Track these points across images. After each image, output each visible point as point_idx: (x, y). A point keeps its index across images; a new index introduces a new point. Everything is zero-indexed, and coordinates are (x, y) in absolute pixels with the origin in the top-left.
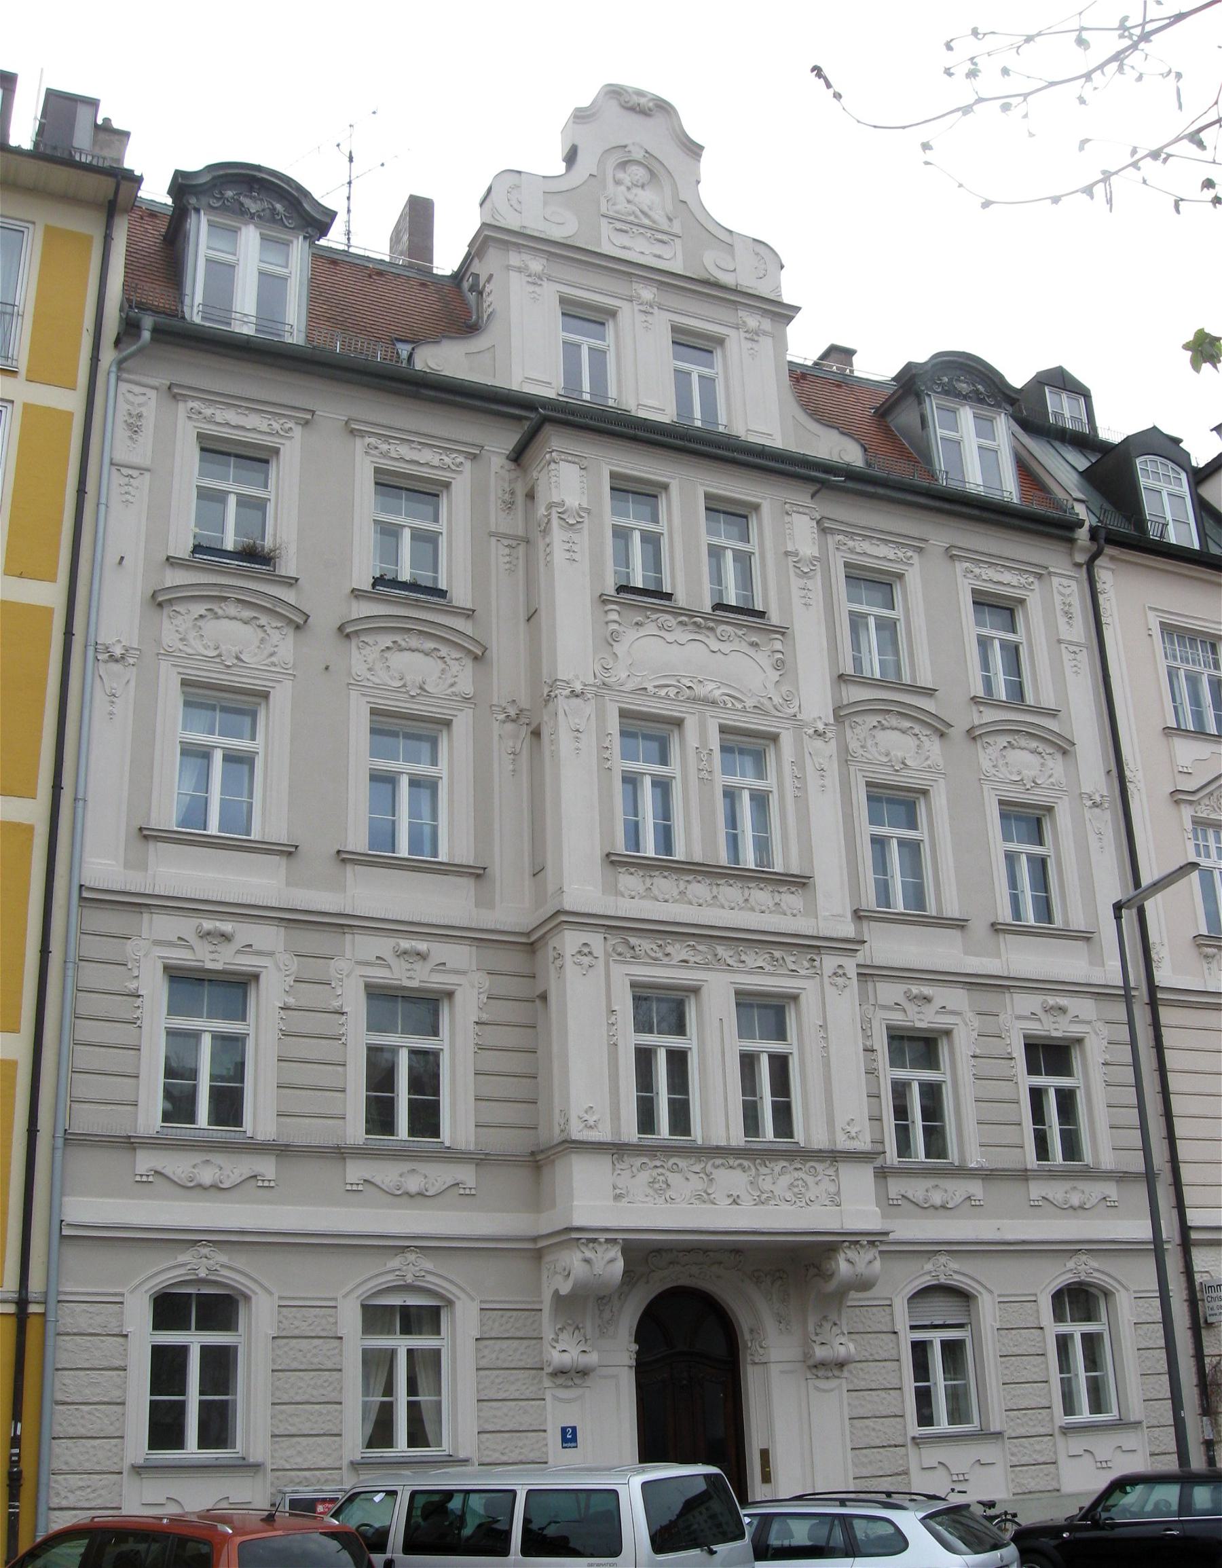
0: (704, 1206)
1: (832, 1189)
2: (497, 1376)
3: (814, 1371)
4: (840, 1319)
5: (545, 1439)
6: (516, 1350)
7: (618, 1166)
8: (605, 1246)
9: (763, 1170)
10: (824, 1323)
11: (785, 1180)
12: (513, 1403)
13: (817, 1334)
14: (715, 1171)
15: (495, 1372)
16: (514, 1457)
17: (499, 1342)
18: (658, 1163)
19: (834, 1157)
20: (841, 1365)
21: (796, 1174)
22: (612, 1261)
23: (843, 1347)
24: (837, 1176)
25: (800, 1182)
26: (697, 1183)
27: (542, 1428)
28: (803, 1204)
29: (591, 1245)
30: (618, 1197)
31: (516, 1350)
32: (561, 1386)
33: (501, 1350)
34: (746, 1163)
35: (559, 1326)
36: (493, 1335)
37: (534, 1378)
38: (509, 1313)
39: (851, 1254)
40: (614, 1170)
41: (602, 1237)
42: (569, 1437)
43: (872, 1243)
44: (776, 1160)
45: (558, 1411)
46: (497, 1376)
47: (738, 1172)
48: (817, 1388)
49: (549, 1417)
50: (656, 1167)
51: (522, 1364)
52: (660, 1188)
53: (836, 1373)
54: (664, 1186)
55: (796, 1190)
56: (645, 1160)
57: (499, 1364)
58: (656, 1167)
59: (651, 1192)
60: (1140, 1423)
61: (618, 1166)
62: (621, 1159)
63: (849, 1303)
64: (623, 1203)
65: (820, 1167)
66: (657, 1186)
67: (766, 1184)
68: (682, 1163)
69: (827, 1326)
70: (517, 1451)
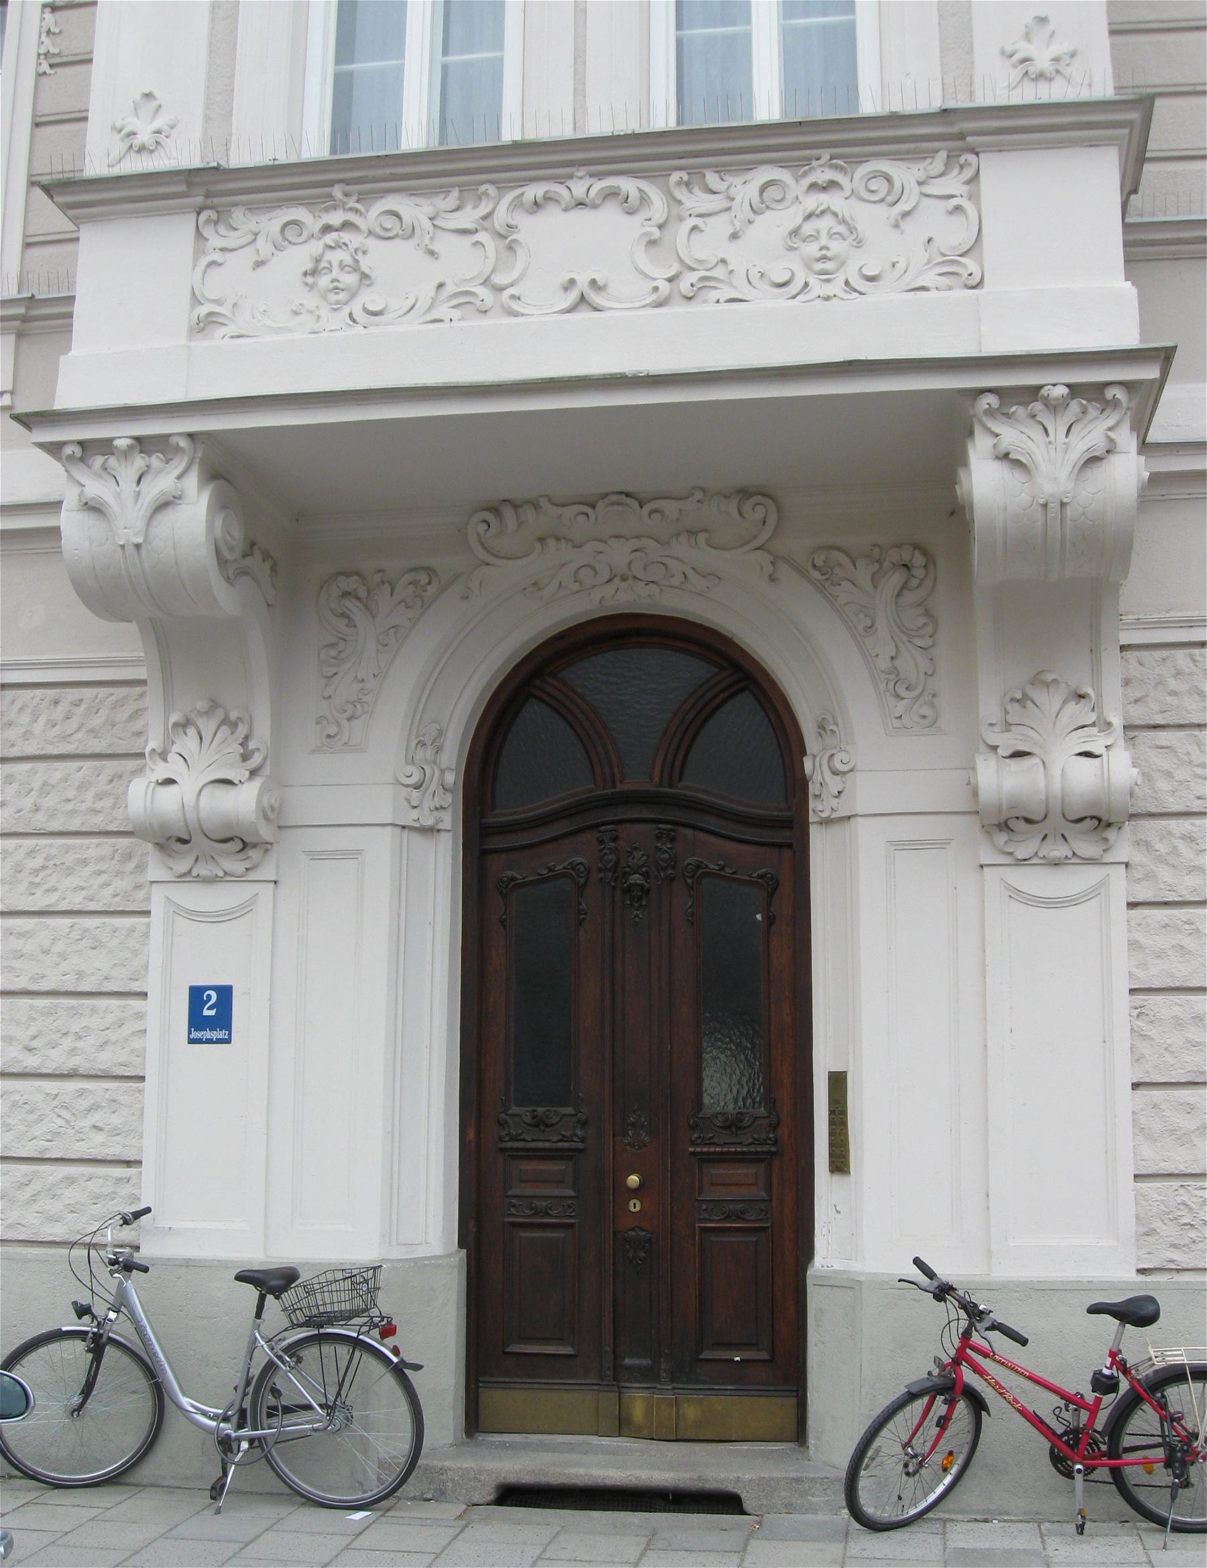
0: (484, 322)
1: (956, 234)
2: (31, 853)
3: (1001, 838)
4: (1097, 686)
5: (140, 1016)
6: (83, 786)
7: (215, 241)
8: (139, 462)
9: (696, 201)
10: (1039, 695)
11: (774, 225)
12: (67, 921)
13: (1007, 726)
14: (523, 221)
15: (29, 843)
16: (56, 1059)
17: (42, 766)
18: (336, 218)
19: (957, 134)
20: (1099, 821)
21: (814, 201)
22: (164, 505)
23: (1077, 761)
24: (974, 197)
25: (825, 223)
26: (462, 261)
27: (135, 987)
28: (836, 287)
29: (98, 461)
30: (205, 324)
31: (83, 786)
32: (185, 877)
33: (46, 788)
34: (628, 185)
35: (175, 718)
36: (31, 749)
37: (129, 857)
38: (74, 694)
39: (1010, 435)
40: (199, 252)
41: (122, 433)
42: (210, 1014)
43: (1094, 393)
44: (749, 167)
45: (189, 936)
46: (31, 853)
47: (610, 213)
48: (1015, 894)
49: (156, 962)
50: (327, 229)
51: (97, 822)
52: (341, 288)
53: (1087, 848)
54: (350, 279)
55: (812, 249)
56: (299, 213)
57: (40, 821)
58: (327, 229)
59: (310, 300)
60: (59, 504)
61: (215, 241)
62: (222, 218)
63: (1127, 638)
64: (218, 339)
65: (904, 174)
66: (324, 281)
67: (708, 245)
68: (413, 210)
69: (1050, 701)
70: (67, 1043)
